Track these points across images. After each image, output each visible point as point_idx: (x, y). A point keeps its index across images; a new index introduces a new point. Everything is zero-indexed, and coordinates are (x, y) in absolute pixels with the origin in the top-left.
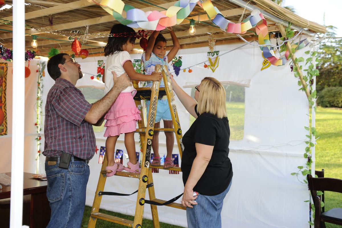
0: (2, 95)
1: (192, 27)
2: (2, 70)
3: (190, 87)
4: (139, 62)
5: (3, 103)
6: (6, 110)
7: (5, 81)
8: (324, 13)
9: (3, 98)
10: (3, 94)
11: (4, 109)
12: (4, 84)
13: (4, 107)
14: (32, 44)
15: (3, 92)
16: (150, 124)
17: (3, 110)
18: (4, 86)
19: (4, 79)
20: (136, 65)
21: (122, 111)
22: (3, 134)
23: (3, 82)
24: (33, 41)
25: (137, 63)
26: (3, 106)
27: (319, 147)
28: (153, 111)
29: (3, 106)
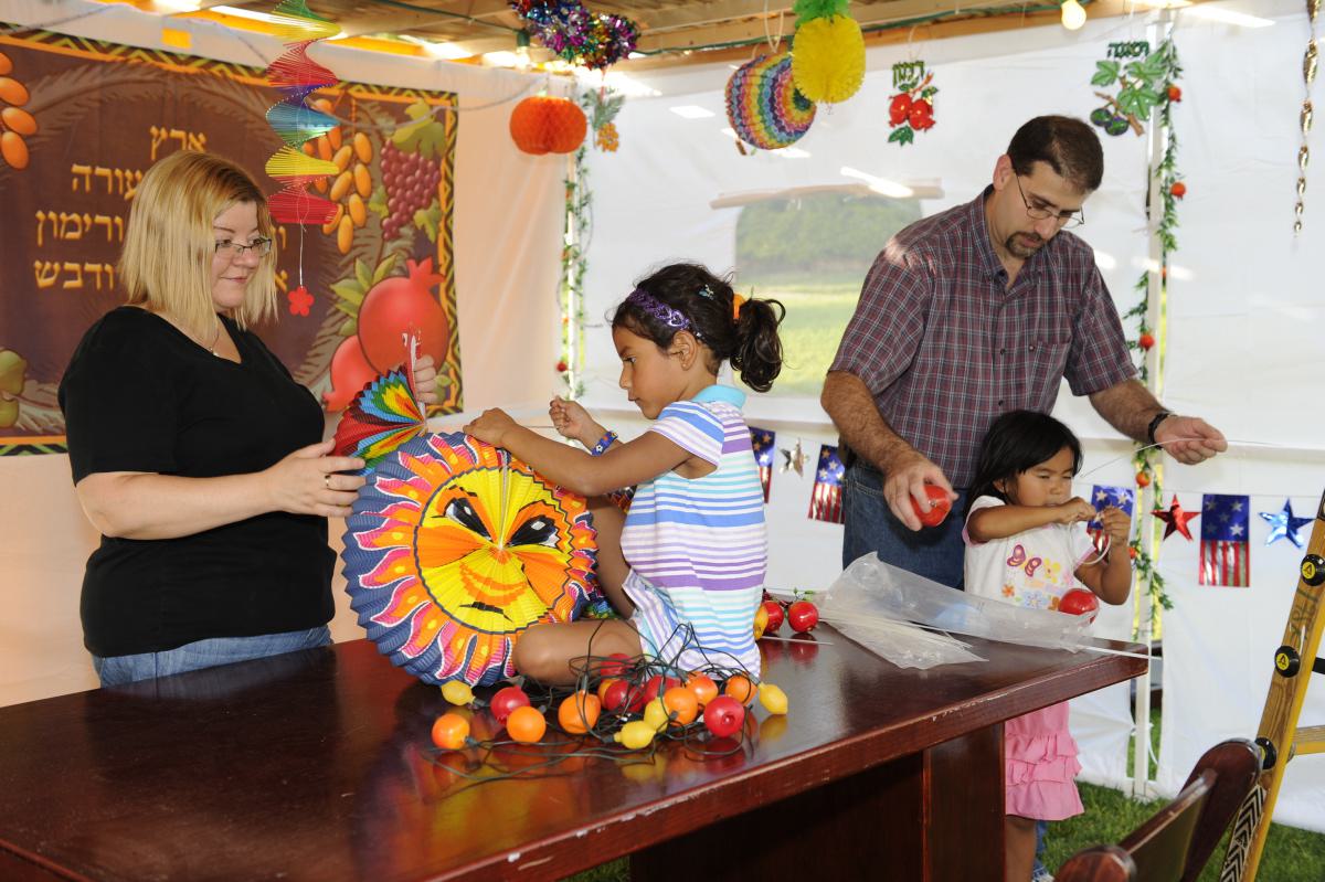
0: (436, 241)
2: (438, 125)
4: (1136, 55)
5: (443, 271)
6: (454, 304)
10: (443, 234)
11: (449, 298)
13: (447, 290)
15: (442, 225)
17: (445, 303)
18: (443, 196)
19: (443, 166)
20: (1121, 73)
23: (439, 180)
25: (1125, 61)
26: (443, 286)
29: (443, 286)
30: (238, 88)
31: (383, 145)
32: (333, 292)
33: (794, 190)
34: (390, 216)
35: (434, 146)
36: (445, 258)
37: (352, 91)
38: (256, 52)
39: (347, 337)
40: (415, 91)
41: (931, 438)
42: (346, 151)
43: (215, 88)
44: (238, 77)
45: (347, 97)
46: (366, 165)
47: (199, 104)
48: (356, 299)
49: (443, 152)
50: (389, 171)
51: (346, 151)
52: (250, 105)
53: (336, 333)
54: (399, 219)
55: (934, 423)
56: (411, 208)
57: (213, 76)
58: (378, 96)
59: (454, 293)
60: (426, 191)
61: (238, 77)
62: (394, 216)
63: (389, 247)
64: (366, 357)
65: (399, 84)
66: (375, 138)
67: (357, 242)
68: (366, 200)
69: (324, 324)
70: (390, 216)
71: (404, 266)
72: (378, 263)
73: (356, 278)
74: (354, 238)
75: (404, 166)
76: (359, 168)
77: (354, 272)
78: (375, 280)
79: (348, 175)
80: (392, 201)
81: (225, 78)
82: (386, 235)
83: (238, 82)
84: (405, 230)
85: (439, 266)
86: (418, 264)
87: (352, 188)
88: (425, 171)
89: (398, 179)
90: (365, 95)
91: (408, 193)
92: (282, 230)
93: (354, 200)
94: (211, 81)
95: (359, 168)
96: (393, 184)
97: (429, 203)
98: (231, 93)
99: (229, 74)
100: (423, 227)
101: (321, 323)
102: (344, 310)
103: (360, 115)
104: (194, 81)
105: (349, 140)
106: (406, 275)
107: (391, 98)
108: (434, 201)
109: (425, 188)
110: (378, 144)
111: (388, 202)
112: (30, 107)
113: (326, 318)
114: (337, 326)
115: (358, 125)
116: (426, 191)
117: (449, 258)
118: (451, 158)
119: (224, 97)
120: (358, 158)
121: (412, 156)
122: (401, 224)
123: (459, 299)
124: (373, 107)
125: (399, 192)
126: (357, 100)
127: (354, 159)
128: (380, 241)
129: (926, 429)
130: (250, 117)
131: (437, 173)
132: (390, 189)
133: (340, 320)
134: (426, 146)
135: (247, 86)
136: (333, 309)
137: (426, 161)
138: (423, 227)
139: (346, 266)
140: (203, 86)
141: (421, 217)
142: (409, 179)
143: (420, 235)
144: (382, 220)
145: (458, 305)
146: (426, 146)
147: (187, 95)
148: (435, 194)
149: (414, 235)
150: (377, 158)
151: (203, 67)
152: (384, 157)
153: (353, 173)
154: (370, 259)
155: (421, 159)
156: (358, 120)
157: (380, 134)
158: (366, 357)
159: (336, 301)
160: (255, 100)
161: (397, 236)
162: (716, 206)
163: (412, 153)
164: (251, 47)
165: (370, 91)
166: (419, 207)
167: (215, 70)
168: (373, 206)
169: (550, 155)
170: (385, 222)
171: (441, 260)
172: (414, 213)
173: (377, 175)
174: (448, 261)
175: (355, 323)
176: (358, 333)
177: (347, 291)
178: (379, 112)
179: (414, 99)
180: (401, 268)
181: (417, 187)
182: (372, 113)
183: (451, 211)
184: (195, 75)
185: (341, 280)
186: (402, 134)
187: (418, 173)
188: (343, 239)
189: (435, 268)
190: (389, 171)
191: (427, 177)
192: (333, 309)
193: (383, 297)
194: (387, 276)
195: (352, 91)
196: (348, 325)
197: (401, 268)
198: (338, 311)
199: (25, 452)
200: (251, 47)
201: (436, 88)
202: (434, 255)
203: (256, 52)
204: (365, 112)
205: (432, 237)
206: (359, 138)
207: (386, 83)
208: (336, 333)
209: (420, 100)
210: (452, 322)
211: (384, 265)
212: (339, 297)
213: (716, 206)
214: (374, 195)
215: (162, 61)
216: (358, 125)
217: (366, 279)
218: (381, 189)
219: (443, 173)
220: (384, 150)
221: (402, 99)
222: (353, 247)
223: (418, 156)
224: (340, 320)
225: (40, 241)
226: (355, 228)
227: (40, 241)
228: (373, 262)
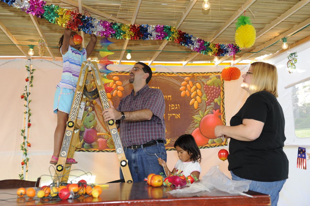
0: (220, 105)
1: (31, 51)
2: (219, 79)
3: (72, 170)
5: (222, 112)
6: (225, 120)
7: (223, 90)
8: (108, 112)
9: (221, 107)
10: (222, 103)
11: (223, 118)
12: (222, 93)
13: (223, 116)
14: (283, 46)
15: (221, 101)
16: (72, 112)
17: (222, 119)
18: (222, 95)
19: (221, 88)
21: (30, 60)
22: (224, 145)
23: (220, 91)
24: (284, 44)
26: (222, 116)
27: (112, 33)
28: (76, 106)
29: (222, 116)
30: (166, 77)
31: (204, 85)
32: (193, 118)
33: (303, 80)
34: (208, 100)
35: (218, 84)
36: (222, 109)
37: (195, 75)
38: (169, 69)
39: (196, 128)
40: (211, 72)
41: (157, 133)
42: (194, 87)
43: (161, 78)
44: (166, 75)
45: (193, 76)
46: (200, 89)
47: (158, 81)
48: (199, 119)
49: (220, 85)
50: (207, 90)
51: (194, 87)
52: (170, 80)
53: (194, 127)
54: (210, 101)
55: (150, 130)
56: (213, 98)
57: (161, 75)
58: (201, 75)
59: (225, 117)
60: (217, 94)
61: (166, 75)
62: (209, 100)
63: (208, 107)
64: (201, 133)
65: (207, 72)
66: (202, 83)
67: (199, 106)
68: (201, 97)
69: (190, 125)
70: (208, 100)
71: (212, 111)
72: (205, 111)
73: (200, 115)
74: (199, 105)
75: (210, 89)
76: (198, 90)
77: (199, 113)
78: (204, 115)
79: (195, 92)
80: (208, 97)
81: (163, 75)
82: (207, 105)
83: (166, 76)
84: (212, 103)
85: (221, 111)
86: (215, 111)
87: (197, 95)
88: (216, 89)
89: (209, 92)
90: (198, 75)
91: (212, 95)
92: (178, 105)
93: (198, 97)
94: (160, 76)
95: (198, 90)
96: (208, 93)
97: (218, 97)
98: (165, 78)
99: (164, 74)
100: (217, 102)
101: (189, 125)
102: (196, 121)
103: (197, 79)
104: (156, 77)
105: (195, 85)
106: (213, 113)
107: (205, 75)
108: (219, 96)
109: (217, 94)
110: (202, 85)
111: (207, 97)
112: (123, 86)
113: (191, 124)
114: (194, 125)
115: (197, 81)
116: (217, 94)
117: (223, 109)
118: (223, 86)
119: (163, 79)
120: (198, 88)
121: (212, 87)
122: (211, 102)
123: (226, 118)
124: (200, 77)
125: (210, 95)
126: (196, 76)
127: (197, 88)
128: (206, 106)
129: (155, 132)
130: (170, 83)
131: (220, 90)
132: (207, 94)
133: (195, 124)
134: (216, 84)
135: (169, 76)
136: (193, 122)
137: (216, 88)
138: (217, 102)
139: (197, 112)
140: (158, 78)
141: (216, 100)
142: (212, 92)
143: (216, 104)
144: (206, 101)
145: (226, 120)
146: (216, 84)
147: (155, 80)
148: (220, 95)
149: (214, 104)
150: (203, 88)
151: (158, 74)
152: (205, 87)
153: (196, 91)
154: (203, 110)
155: (215, 87)
156: (197, 80)
157: (203, 83)
158: (201, 133)
159: (194, 120)
160: (171, 79)
161: (210, 105)
162: (286, 88)
163: (212, 86)
164: (57, 65)
165: (199, 74)
166: (215, 98)
167: (161, 74)
168: (203, 98)
169: (232, 81)
170: (207, 102)
171: (221, 110)
172: (214, 99)
173: (203, 91)
174: (223, 110)
175: (199, 125)
176: (199, 127)
177: (197, 118)
178: (202, 78)
179: (211, 74)
180: (211, 112)
181: (215, 93)
182: (200, 78)
183: (224, 98)
184: (156, 76)
185: (195, 115)
186: (209, 82)
187: (214, 90)
188: (196, 106)
189: (220, 111)
190: (207, 90)
191: (217, 91)
192: (193, 122)
193: (207, 119)
194: (208, 114)
195: (195, 75)
196: (197, 125)
197: (211, 112)
198: (194, 122)
199: (173, 150)
200: (57, 65)
201: (217, 71)
202: (220, 108)
203: (169, 69)
204: (198, 78)
205: (219, 104)
206: (197, 84)
207: (203, 72)
208: (194, 127)
209: (213, 74)
210: (224, 124)
211: (207, 111)
212: (195, 119)
213: (286, 88)
214: (203, 96)
215: (167, 74)
216: (197, 81)
217: (202, 114)
218: (205, 94)
219: (221, 90)
220: (204, 86)
221: (208, 75)
222: (198, 108)
223: (214, 86)
224: (195, 124)
225: (170, 110)
226: (198, 103)
227: (170, 110)
228: (204, 111)
